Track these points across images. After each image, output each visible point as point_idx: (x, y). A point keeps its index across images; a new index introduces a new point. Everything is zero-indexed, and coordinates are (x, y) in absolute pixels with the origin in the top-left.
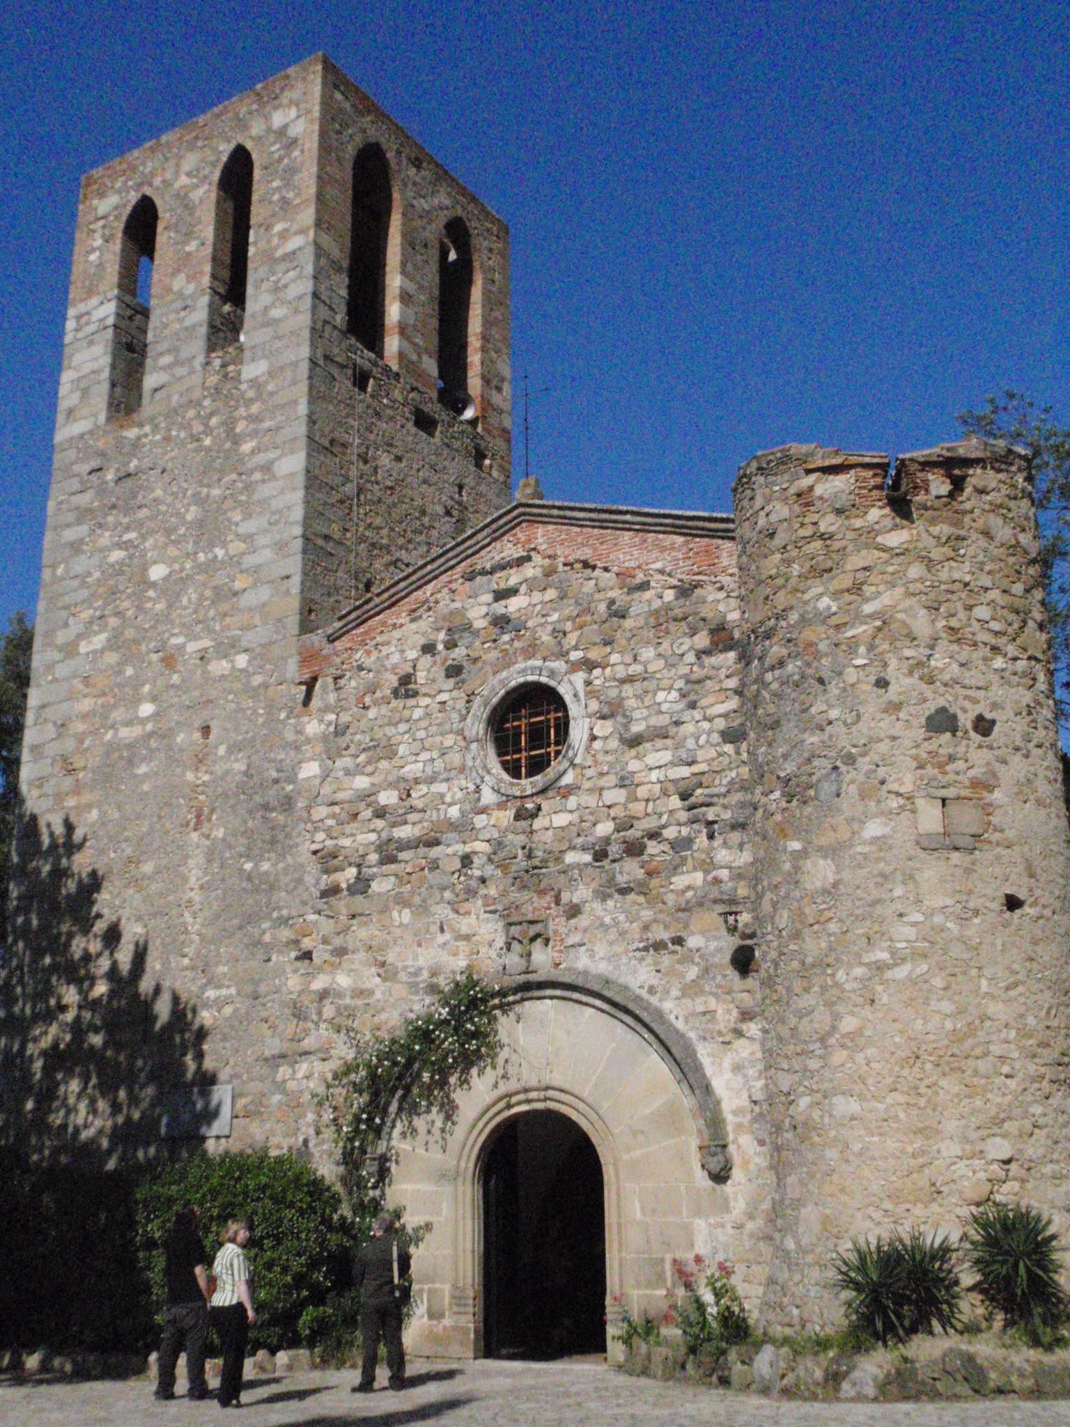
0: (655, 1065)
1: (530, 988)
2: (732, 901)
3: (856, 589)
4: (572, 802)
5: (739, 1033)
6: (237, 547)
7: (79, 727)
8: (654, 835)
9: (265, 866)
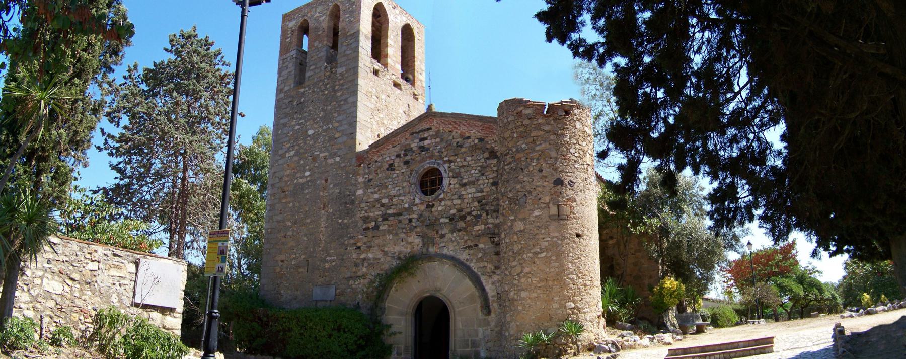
0: (468, 283)
1: (430, 258)
2: (494, 234)
3: (534, 142)
4: (443, 203)
5: (494, 273)
6: (336, 125)
7: (287, 179)
8: (470, 214)
9: (346, 221)
